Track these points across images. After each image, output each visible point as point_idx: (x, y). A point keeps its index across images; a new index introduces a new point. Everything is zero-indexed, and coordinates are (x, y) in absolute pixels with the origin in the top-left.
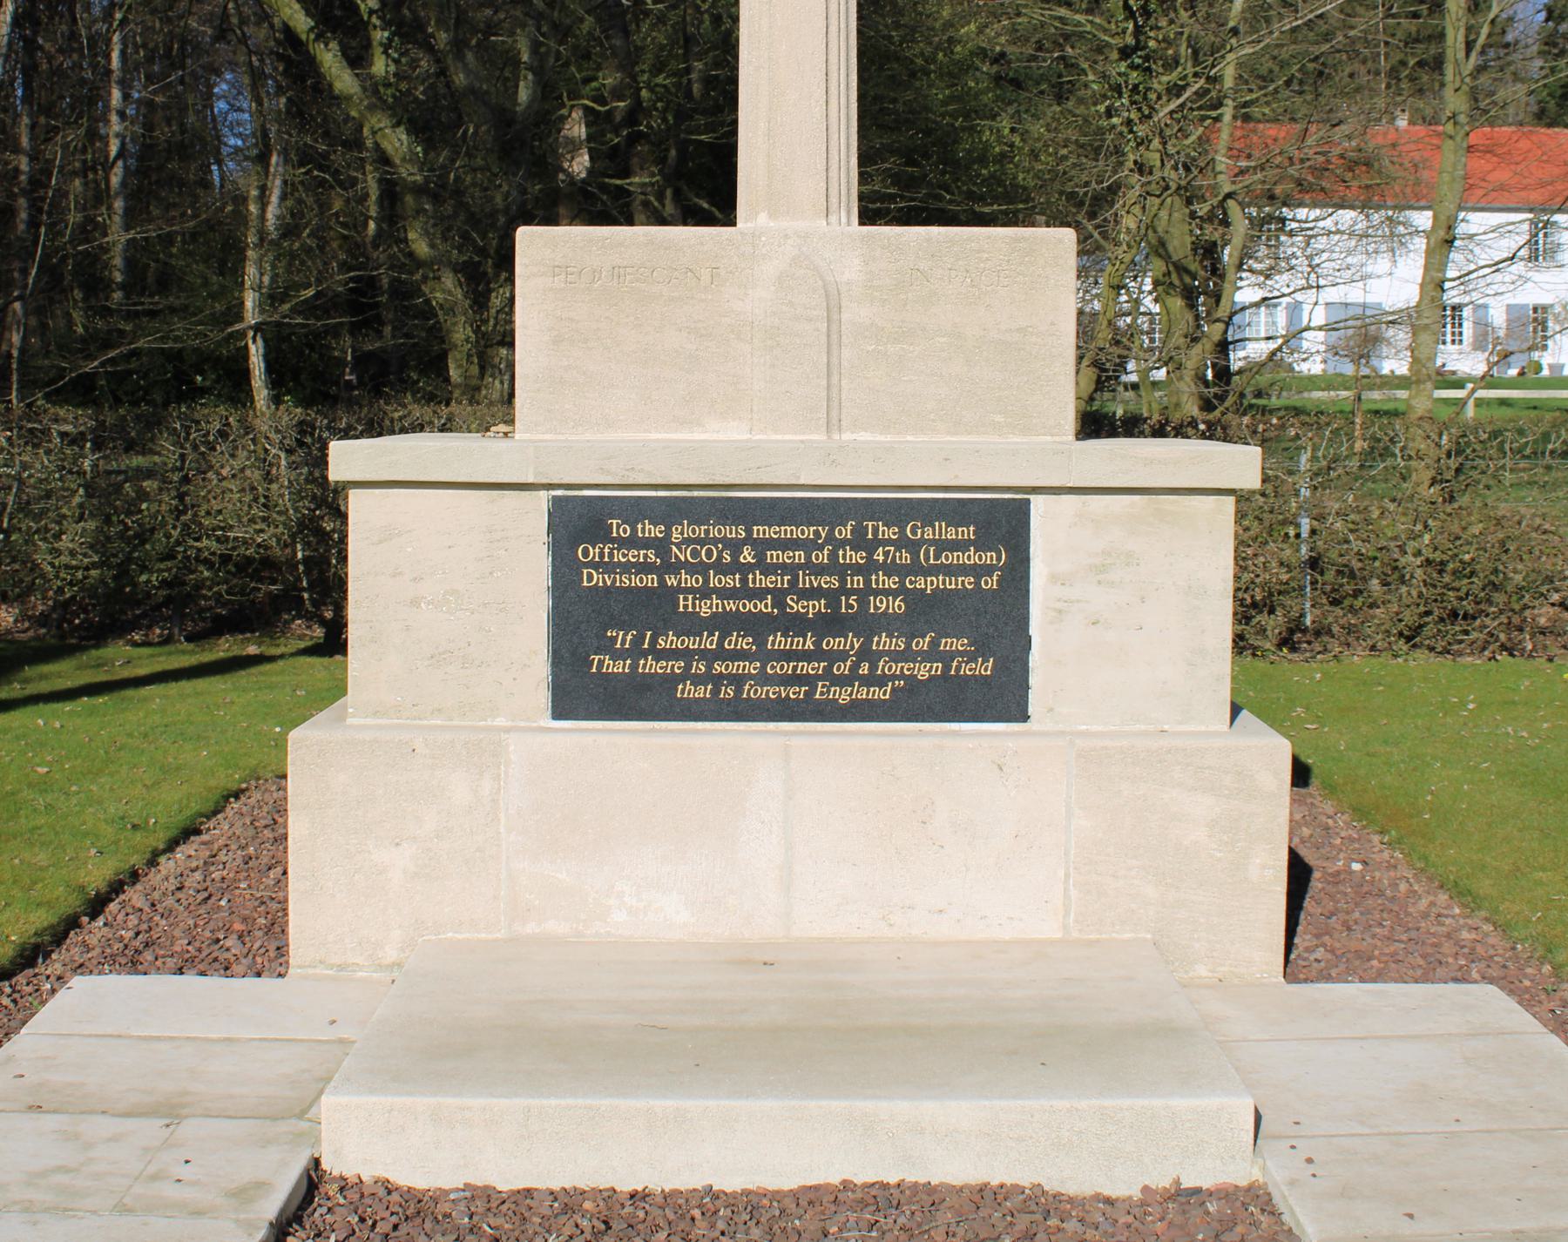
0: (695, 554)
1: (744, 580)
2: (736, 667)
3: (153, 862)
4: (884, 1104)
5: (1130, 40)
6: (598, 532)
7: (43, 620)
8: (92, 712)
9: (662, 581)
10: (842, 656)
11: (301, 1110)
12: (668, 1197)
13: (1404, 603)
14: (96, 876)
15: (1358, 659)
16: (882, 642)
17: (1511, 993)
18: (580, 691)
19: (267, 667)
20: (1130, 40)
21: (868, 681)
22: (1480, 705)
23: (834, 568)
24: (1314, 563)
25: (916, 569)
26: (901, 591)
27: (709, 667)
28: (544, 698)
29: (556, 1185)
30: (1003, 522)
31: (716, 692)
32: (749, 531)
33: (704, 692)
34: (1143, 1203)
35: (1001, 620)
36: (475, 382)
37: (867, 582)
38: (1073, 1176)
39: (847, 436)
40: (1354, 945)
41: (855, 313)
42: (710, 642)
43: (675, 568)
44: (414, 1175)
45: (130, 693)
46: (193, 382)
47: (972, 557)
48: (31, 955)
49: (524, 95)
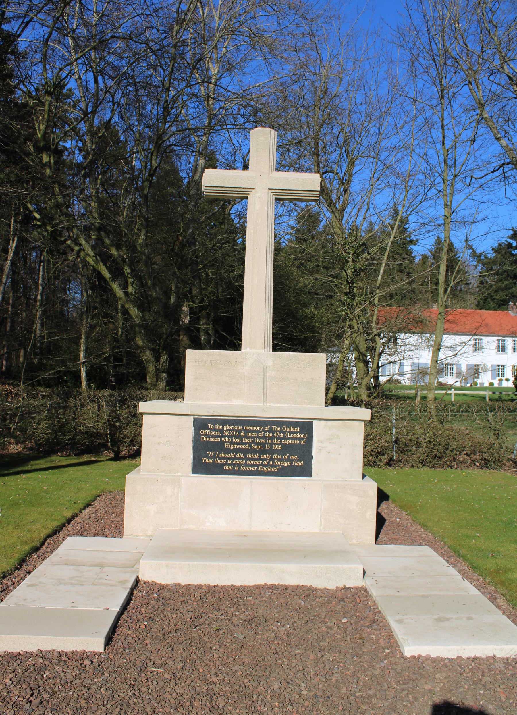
0: (230, 433)
1: (242, 440)
2: (239, 462)
3: (81, 512)
4: (275, 565)
5: (348, 290)
6: (206, 427)
7: (31, 449)
8: (54, 474)
9: (221, 440)
10: (266, 460)
11: (134, 564)
12: (223, 587)
13: (420, 453)
14: (68, 514)
15: (407, 469)
16: (276, 456)
17: (432, 548)
18: (200, 467)
19: (99, 464)
20: (348, 290)
21: (272, 466)
22: (438, 481)
23: (264, 437)
24: (397, 441)
25: (284, 438)
26: (281, 443)
27: (232, 462)
28: (191, 468)
29: (196, 584)
30: (306, 427)
31: (234, 468)
32: (243, 428)
33: (230, 468)
34: (336, 590)
35: (305, 452)
36: (154, 383)
37: (272, 441)
38: (319, 583)
39: (268, 404)
40: (394, 537)
41: (271, 374)
42: (233, 455)
43: (223, 436)
44: (162, 580)
45: (62, 469)
46: (63, 379)
47: (298, 436)
48: (55, 532)
49: (172, 300)
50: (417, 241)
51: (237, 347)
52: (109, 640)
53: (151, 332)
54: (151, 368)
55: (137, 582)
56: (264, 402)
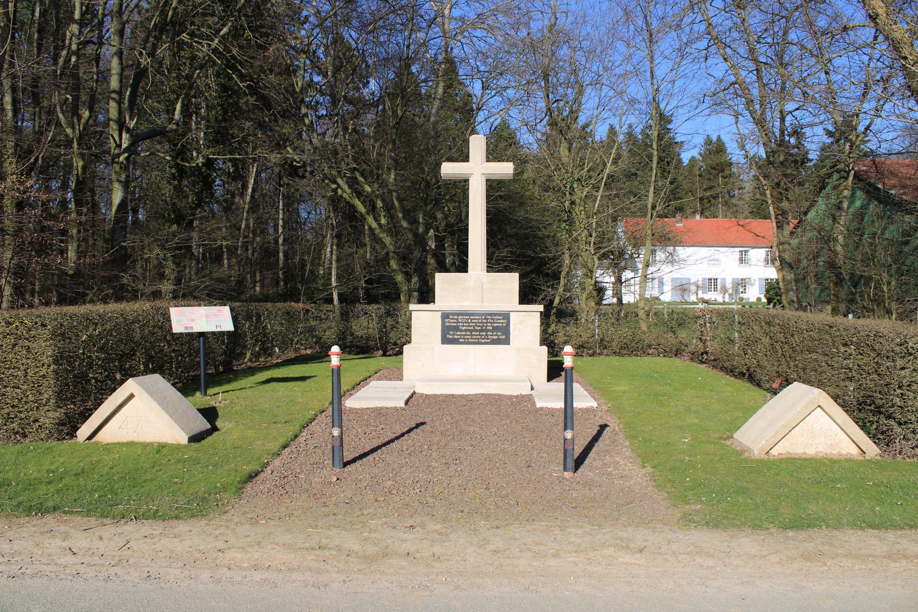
18: (445, 340)
28: (440, 341)
30: (506, 316)
35: (506, 330)
50: (682, 143)
51: (467, 272)
52: (407, 403)
53: (404, 259)
54: (405, 288)
55: (414, 393)
56: (482, 302)
